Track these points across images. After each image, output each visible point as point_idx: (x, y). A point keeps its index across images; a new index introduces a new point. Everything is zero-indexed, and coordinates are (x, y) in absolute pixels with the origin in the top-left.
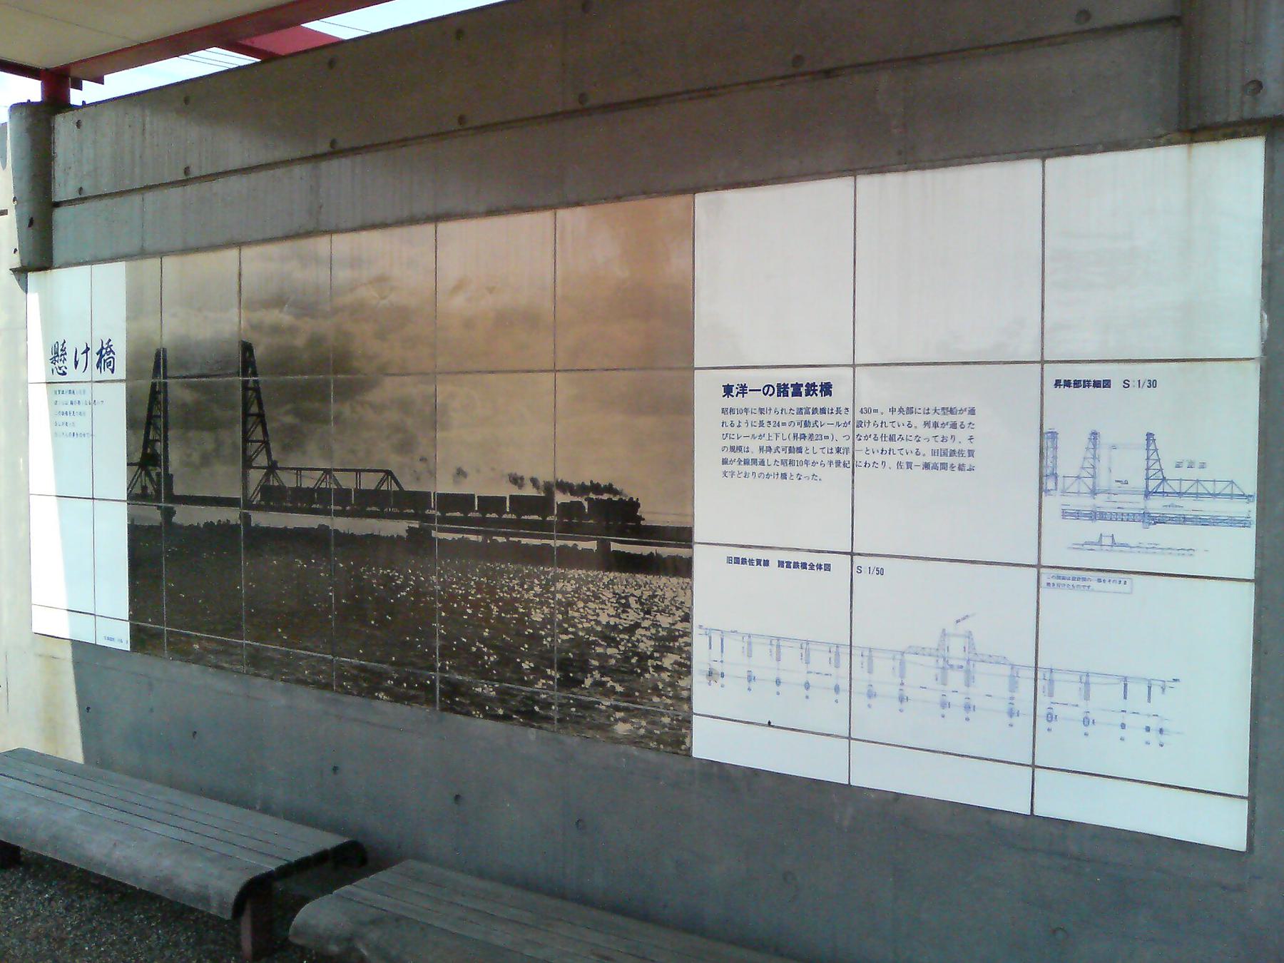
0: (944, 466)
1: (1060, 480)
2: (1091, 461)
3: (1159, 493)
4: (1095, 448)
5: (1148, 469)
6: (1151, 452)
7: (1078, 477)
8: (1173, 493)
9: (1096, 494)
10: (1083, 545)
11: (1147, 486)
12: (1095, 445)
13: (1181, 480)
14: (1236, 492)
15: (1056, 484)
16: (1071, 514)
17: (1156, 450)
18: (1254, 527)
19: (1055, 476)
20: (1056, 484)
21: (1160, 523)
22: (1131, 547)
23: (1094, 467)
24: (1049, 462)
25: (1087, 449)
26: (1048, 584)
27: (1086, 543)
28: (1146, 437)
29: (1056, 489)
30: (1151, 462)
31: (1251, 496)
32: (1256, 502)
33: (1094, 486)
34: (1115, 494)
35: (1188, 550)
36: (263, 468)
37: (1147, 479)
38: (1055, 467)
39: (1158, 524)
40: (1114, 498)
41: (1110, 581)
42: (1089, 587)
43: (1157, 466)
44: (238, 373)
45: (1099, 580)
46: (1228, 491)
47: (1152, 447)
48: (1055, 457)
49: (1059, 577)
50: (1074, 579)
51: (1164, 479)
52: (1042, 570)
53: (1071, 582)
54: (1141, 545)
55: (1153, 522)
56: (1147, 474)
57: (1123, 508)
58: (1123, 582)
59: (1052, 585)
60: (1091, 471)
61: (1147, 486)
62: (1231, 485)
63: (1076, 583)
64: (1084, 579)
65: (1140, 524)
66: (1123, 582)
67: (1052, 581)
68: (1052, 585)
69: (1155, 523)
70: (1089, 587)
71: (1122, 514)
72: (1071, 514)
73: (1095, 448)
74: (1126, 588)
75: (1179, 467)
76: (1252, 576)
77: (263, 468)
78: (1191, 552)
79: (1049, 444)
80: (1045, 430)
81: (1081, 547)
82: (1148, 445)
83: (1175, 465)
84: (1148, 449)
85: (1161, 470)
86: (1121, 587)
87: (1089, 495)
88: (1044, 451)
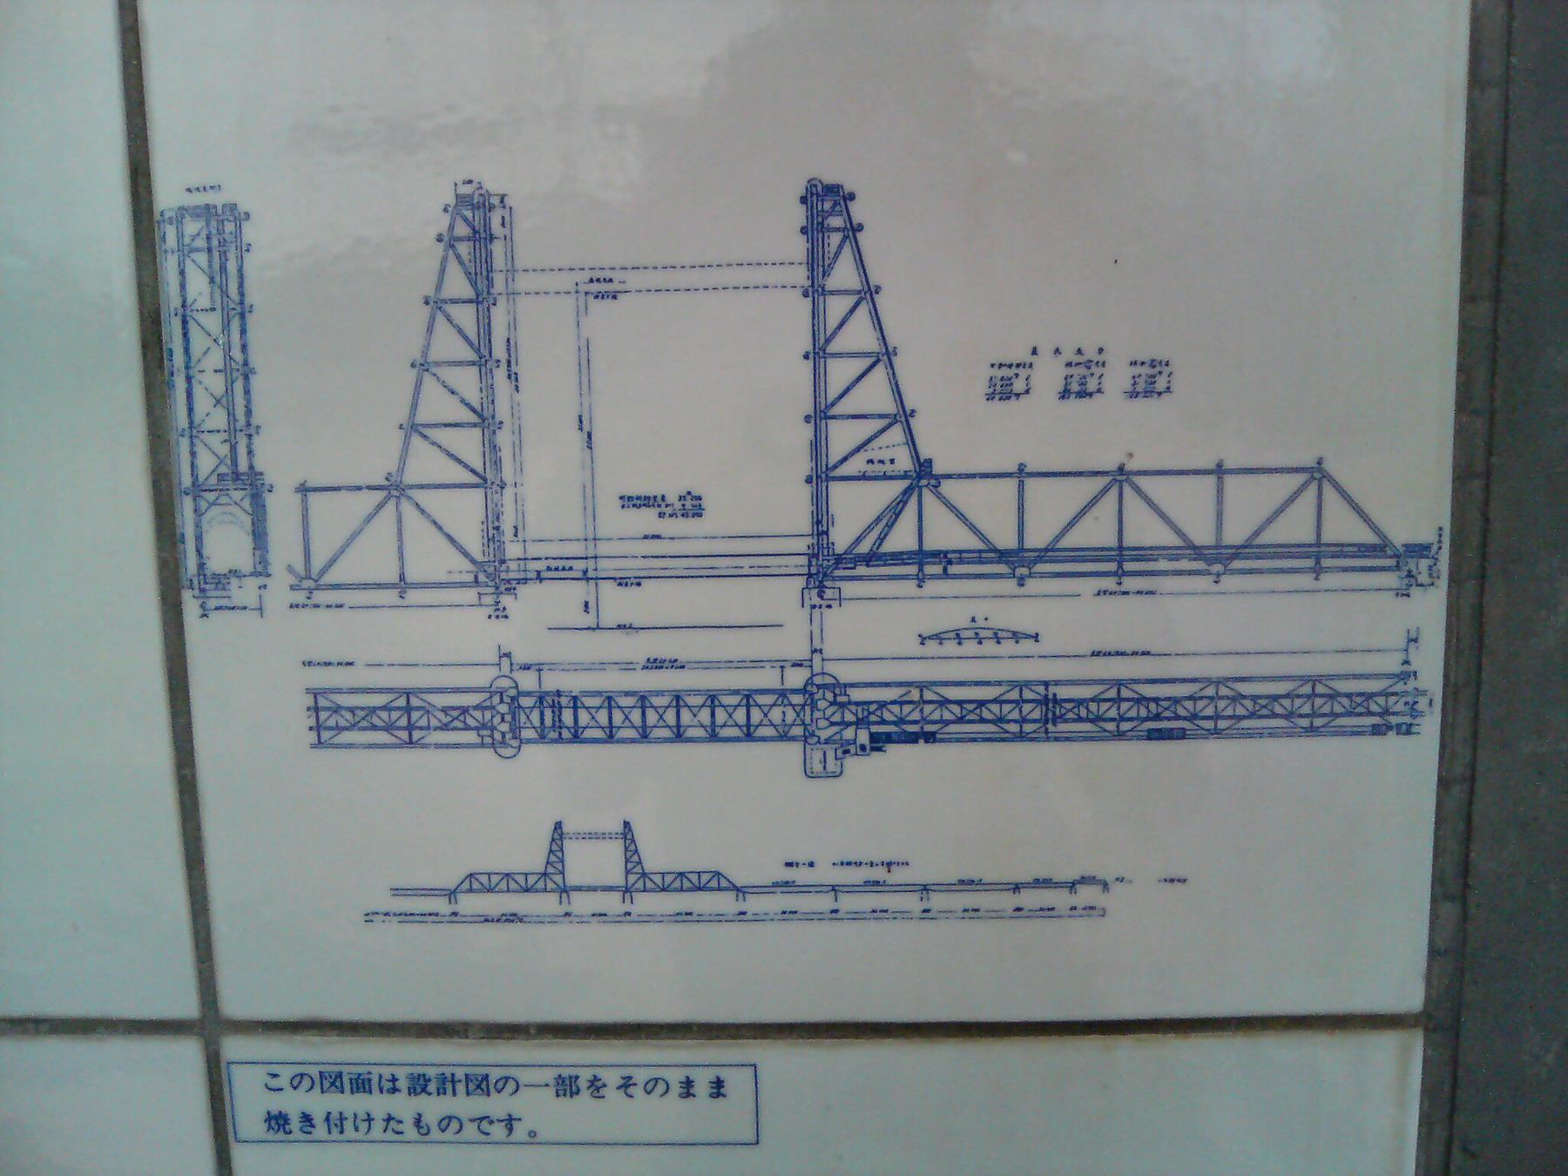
0: (336, 1122)
1: (282, 509)
2: (467, 382)
3: (898, 558)
4: (482, 300)
5: (820, 415)
6: (836, 308)
7: (394, 489)
8: (978, 557)
9: (510, 587)
10: (451, 894)
11: (821, 523)
12: (481, 275)
13: (1021, 474)
14: (1343, 527)
15: (259, 536)
16: (365, 719)
17: (868, 293)
18: (1430, 726)
19: (254, 486)
20: (259, 536)
21: (912, 739)
22: (740, 891)
23: (485, 420)
24: (203, 403)
25: (437, 304)
26: (277, 1121)
27: (474, 882)
28: (798, 215)
29: (262, 569)
30: (840, 373)
31: (1420, 550)
32: (1443, 583)
33: (493, 535)
34: (622, 582)
35: (1072, 886)
36: (835, 355)
37: (822, 476)
38: (243, 428)
39: (893, 749)
40: (616, 603)
41: (626, 1084)
42: (510, 1122)
43: (874, 395)
44: (812, 535)
45: (566, 1086)
46: (1296, 528)
47: (844, 275)
48: (241, 371)
49: (332, 1081)
50: (419, 1085)
51: (923, 475)
52: (234, 1047)
53: (404, 1106)
54: (801, 876)
55: (863, 737)
56: (818, 447)
57: (675, 664)
58: (702, 1088)
59: (295, 1124)
60: (469, 444)
61: (821, 523)
62: (1312, 490)
63: (433, 1107)
64: (480, 1084)
65: (791, 753)
66: (702, 1088)
67: (293, 1103)
68: (295, 1124)
69: (878, 742)
70: (510, 1122)
71: (678, 699)
72: (365, 719)
73: (482, 300)
74: (732, 1116)
75: (1083, 394)
76: (1412, 998)
77: (835, 355)
78: (1087, 895)
79: (198, 287)
80: (168, 194)
81: (441, 905)
82: (817, 264)
83: (983, 387)
84: (816, 291)
85: (903, 416)
86: (700, 1116)
87: (470, 595)
88: (172, 330)
